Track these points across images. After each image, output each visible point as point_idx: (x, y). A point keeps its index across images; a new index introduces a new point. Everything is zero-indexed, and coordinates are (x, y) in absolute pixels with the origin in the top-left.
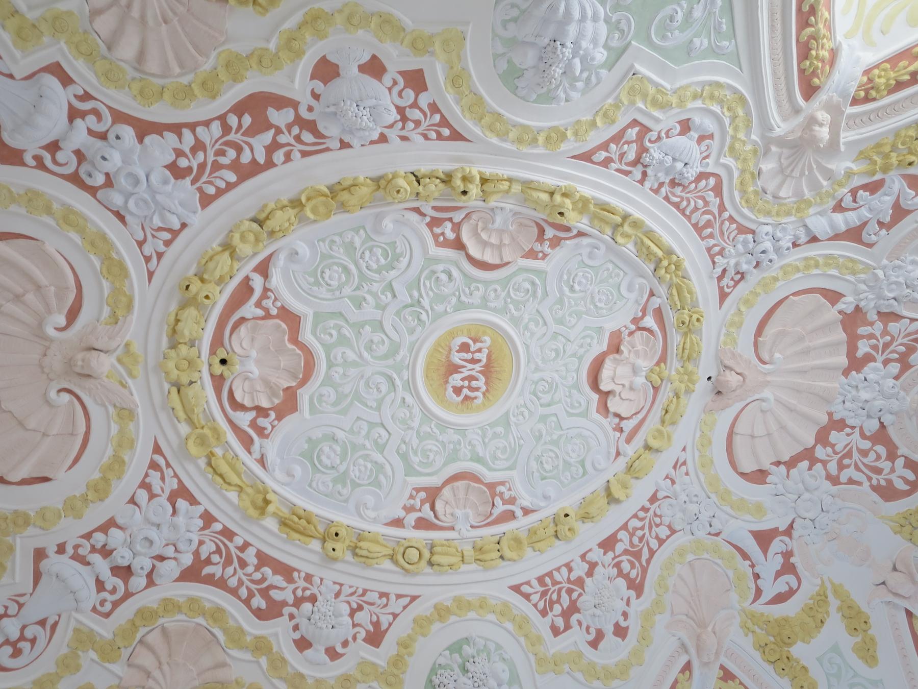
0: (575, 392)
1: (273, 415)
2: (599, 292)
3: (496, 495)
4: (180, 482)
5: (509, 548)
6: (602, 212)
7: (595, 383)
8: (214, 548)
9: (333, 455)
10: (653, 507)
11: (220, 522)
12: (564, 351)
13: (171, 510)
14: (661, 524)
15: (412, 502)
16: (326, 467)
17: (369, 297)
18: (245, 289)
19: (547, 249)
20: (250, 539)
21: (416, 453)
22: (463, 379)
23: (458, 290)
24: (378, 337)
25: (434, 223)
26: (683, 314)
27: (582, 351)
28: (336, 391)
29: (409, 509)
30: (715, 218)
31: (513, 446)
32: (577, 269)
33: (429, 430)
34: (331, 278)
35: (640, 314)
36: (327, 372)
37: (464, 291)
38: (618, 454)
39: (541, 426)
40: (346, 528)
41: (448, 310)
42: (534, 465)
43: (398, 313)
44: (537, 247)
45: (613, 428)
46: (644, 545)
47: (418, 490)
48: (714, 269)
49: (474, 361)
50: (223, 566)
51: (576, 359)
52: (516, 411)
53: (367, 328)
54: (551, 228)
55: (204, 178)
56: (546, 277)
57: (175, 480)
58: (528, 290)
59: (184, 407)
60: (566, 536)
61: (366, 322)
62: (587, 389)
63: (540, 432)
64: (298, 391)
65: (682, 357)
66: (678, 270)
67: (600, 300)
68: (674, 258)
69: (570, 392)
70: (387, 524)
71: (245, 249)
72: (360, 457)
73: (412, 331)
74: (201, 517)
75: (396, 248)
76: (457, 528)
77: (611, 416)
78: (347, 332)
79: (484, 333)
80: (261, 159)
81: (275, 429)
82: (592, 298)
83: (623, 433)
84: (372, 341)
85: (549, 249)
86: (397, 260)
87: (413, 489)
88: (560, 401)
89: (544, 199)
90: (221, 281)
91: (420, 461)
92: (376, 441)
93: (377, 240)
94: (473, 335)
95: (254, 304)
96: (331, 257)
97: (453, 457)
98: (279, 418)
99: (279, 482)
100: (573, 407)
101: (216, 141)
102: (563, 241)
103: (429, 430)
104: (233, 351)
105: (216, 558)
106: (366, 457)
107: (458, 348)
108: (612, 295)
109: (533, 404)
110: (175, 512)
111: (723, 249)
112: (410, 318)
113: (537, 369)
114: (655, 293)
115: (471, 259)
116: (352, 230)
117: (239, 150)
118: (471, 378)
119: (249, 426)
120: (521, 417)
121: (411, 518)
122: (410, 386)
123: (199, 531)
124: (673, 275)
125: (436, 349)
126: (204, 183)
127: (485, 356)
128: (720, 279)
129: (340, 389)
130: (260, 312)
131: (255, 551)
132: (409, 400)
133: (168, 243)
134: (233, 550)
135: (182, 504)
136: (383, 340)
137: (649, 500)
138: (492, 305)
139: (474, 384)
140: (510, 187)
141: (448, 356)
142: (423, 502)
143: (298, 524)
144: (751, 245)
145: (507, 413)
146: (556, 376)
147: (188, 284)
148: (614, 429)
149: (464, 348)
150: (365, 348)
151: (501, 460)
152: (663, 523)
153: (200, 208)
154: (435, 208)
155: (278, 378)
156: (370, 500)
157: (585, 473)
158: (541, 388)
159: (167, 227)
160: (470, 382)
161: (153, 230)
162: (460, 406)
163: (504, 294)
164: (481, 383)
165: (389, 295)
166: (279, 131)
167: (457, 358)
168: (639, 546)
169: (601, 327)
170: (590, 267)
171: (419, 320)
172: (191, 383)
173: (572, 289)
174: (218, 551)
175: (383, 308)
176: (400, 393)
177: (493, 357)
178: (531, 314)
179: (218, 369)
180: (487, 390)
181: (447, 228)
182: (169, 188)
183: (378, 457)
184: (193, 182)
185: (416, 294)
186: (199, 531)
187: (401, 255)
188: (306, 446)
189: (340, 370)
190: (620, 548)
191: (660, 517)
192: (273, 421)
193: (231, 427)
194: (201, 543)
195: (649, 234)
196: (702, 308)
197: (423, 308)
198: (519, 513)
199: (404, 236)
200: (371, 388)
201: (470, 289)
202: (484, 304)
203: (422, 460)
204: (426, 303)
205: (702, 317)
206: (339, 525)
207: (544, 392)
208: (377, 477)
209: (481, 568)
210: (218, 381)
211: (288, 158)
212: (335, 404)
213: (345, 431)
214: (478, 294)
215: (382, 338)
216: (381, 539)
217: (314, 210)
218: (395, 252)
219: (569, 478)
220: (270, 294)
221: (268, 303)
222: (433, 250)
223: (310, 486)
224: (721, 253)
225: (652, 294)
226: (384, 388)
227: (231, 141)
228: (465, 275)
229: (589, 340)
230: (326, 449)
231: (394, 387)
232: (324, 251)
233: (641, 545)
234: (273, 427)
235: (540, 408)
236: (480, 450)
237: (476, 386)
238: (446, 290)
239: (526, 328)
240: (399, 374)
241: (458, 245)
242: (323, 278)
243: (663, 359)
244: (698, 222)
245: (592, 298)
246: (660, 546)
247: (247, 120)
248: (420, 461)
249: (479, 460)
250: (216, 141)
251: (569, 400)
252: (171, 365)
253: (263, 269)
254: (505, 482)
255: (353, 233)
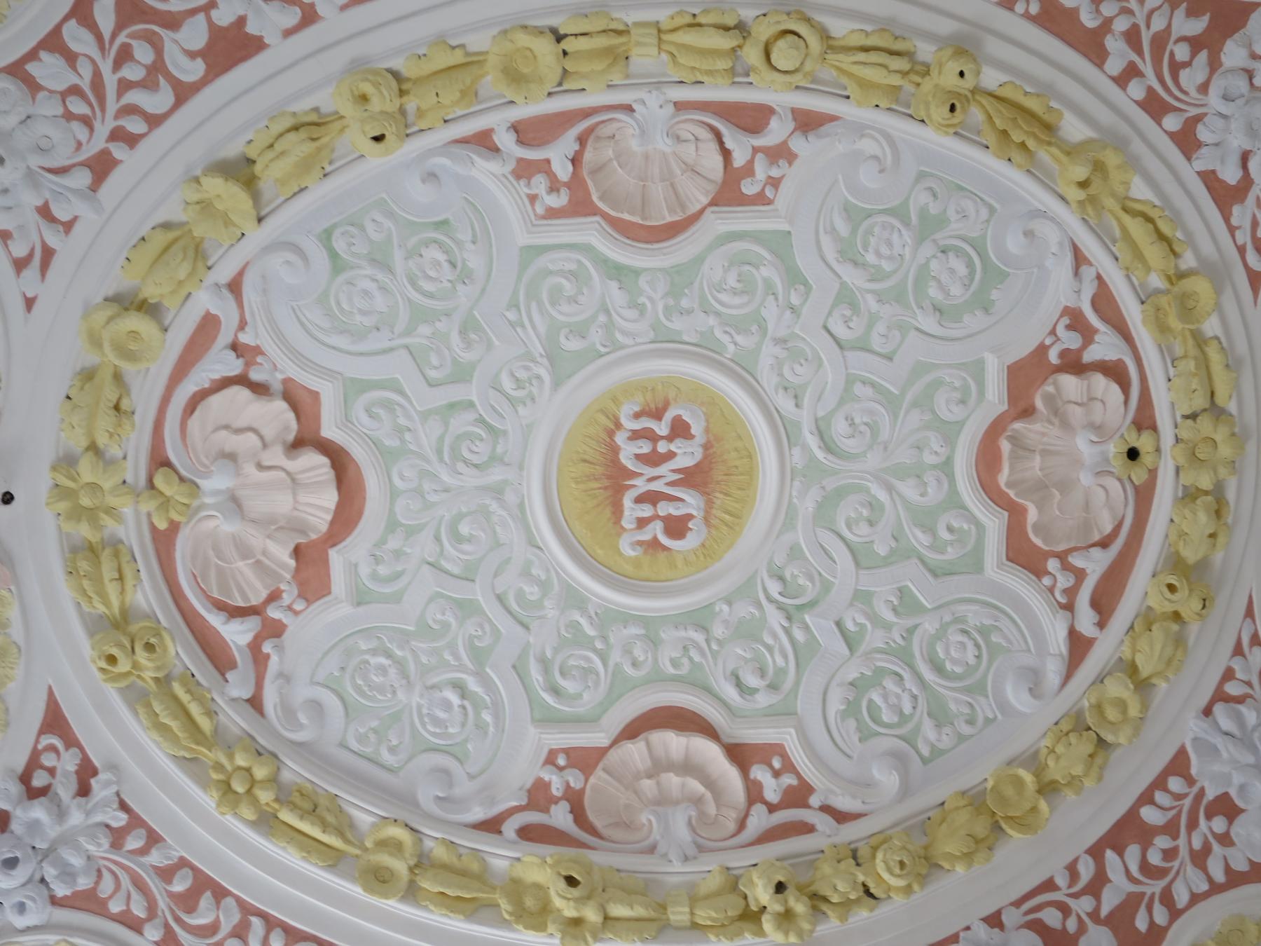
0: (387, 442)
1: (1053, 357)
2: (394, 692)
3: (567, 185)
4: (1227, 219)
5: (535, 57)
6: (474, 895)
7: (339, 459)
8: (1184, 75)
9: (944, 278)
10: (99, 142)
11: (1166, 131)
12: (437, 538)
13: (1252, 165)
14: (64, 95)
15: (775, 173)
16: (959, 252)
17: (888, 616)
18: (1103, 605)
19: (549, 775)
20: (1113, 90)
21: (769, 285)
22: (671, 455)
23: (715, 655)
24: (860, 533)
25: (798, 795)
26: (158, 669)
27: (393, 543)
28: (934, 412)
29: (783, 153)
30: (178, 920)
31: (534, 305)
32: (466, 740)
33: (739, 339)
34: (963, 645)
35: (267, 648)
36: (953, 451)
37: (703, 654)
38: (235, 287)
39: (467, 357)
40: (929, 116)
41: (725, 608)
42: (474, 261)
43: (827, 587)
44: (575, 779)
45: (262, 353)
46: (114, 36)
47: (760, 199)
48: (118, 794)
49: (651, 498)
50: (1169, 34)
51: (403, 521)
52: (535, 391)
53: (882, 550)
54: (563, 830)
55: (1187, 802)
56: (532, 709)
57: (1234, 221)
58: (562, 674)
59: (1208, 368)
60: (376, 85)
61: (887, 561)
62: (358, 452)
63: (468, 345)
64: (1005, 407)
65: (116, 555)
66: (223, 781)
67: (383, 670)
68: (249, 814)
69: (402, 441)
70: (833, 118)
71: (1118, 688)
72: (888, 276)
73: (794, 553)
74: (1199, 145)
75: (859, 729)
76: (670, 109)
77: (277, 386)
78: (919, 539)
79: (636, 563)
80: (1110, 855)
81: (1050, 327)
82: (404, 674)
83: (229, 339)
84: (871, 523)
85: (547, 779)
86: (849, 703)
87: (770, 202)
88: (425, 416)
89: (619, 906)
90: (1147, 619)
91: (757, 268)
92: (854, 306)
93: (896, 740)
94: (662, 556)
95: (1087, 575)
96: (967, 690)
97: (680, 279)
98: (1042, 349)
99: (1052, 219)
100: (388, 405)
101: (1178, 873)
102: (524, 803)
103: (739, 339)
104: (1120, 480)
105: (1182, 52)
106: (877, 275)
107: (690, 525)
108: (358, 689)
109: (492, 407)
110: (1245, 158)
111: (116, 845)
112: (801, 581)
113: (497, 491)
114: (248, 706)
115: (709, 731)
116: (942, 752)
117: (1145, 867)
118: (654, 459)
119: (1096, 331)
120: (522, 375)
121: (777, 130)
122: (785, 433)
123: (1206, 114)
124: (229, 768)
125: (737, 520)
126: (1186, 795)
127: (627, 513)
128: (86, 772)
129: (928, 417)
130: (1077, 561)
131: (1107, 66)
132: (785, 404)
133: (1229, 675)
134: (1148, 69)
135: (1231, 175)
136: (849, 527)
137: (115, 163)
138: (634, 630)
139: (645, 448)
140: (692, 914)
141: (709, 504)
142: (749, 170)
143: (1026, 132)
144: (50, 872)
145: (557, 384)
146: (446, 477)
147: (1203, 611)
148: (257, 350)
149: (677, 527)
150: (882, 508)
151: (561, 273)
152: (59, 96)
153: (1189, 749)
154: (808, 829)
155: (1044, 434)
156: (868, 177)
157: (326, 237)
158: (481, 447)
159: (1232, 705)
160: (654, 450)
161: (1251, 696)
162: (671, 395)
163: (616, 657)
164: (628, 452)
165: (850, 626)
166: (1094, 915)
167: (691, 502)
168: (129, 36)
169: (359, 604)
170: (435, 749)
171: (781, 579)
172: (1193, 417)
173: (459, 687)
174: (1176, 67)
175: (862, 597)
176: (805, 419)
177: (608, 512)
178: (540, 618)
179: (1144, 443)
180: (611, 434)
181: (772, 789)
182: (1237, 779)
183: (851, 276)
184: (1201, 793)
185: (799, 635)
186: (1206, 114)
187: (844, 715)
188: (995, 295)
189: (929, 459)
190: (195, 34)
191: (69, 116)
192: (1053, 344)
193: (1128, 328)
194: (1204, 88)
195: (333, 860)
196: (111, 692)
197: (781, 607)
198: (506, 140)
199: (849, 756)
200: (866, 424)
201: (691, 659)
202: (651, 627)
203: (754, 271)
204: (775, 618)
205: (102, 670)
206: (943, 127)
207: (470, 436)
208: (854, 231)
209: (615, 15)
210: (1144, 421)
211: (1072, 870)
212: (937, 384)
213: (917, 329)
214: (667, 654)
215: (852, 533)
216: (852, 90)
217: (1018, 783)
218: (857, 720)
219: (370, 228)
220: (1063, 600)
221: (1064, 581)
222: (788, 737)
223: (992, 210)
224: (117, 837)
225: (255, 703)
226: (839, 427)
227: (1158, 879)
228: (708, 690)
229: (383, 570)
230: (956, 290)
231: (818, 428)
232: (982, 699)
233: (122, 38)
234: (1053, 332)
235: (475, 399)
236: (617, 296)
237: (641, 442)
238: (740, 652)
239: (544, 585)
240: (812, 458)
241: (739, 755)
242: (977, 646)
243: (164, 541)
244: (218, 903)
245: (404, 674)
246: (57, 30)
247: (1141, 924)
248: (757, 268)
249: (617, 272)
250: (1178, 873)
251: (402, 421)
252: (1225, 451)
253: (1078, 646)
254: (544, 217)
255: (941, 746)
